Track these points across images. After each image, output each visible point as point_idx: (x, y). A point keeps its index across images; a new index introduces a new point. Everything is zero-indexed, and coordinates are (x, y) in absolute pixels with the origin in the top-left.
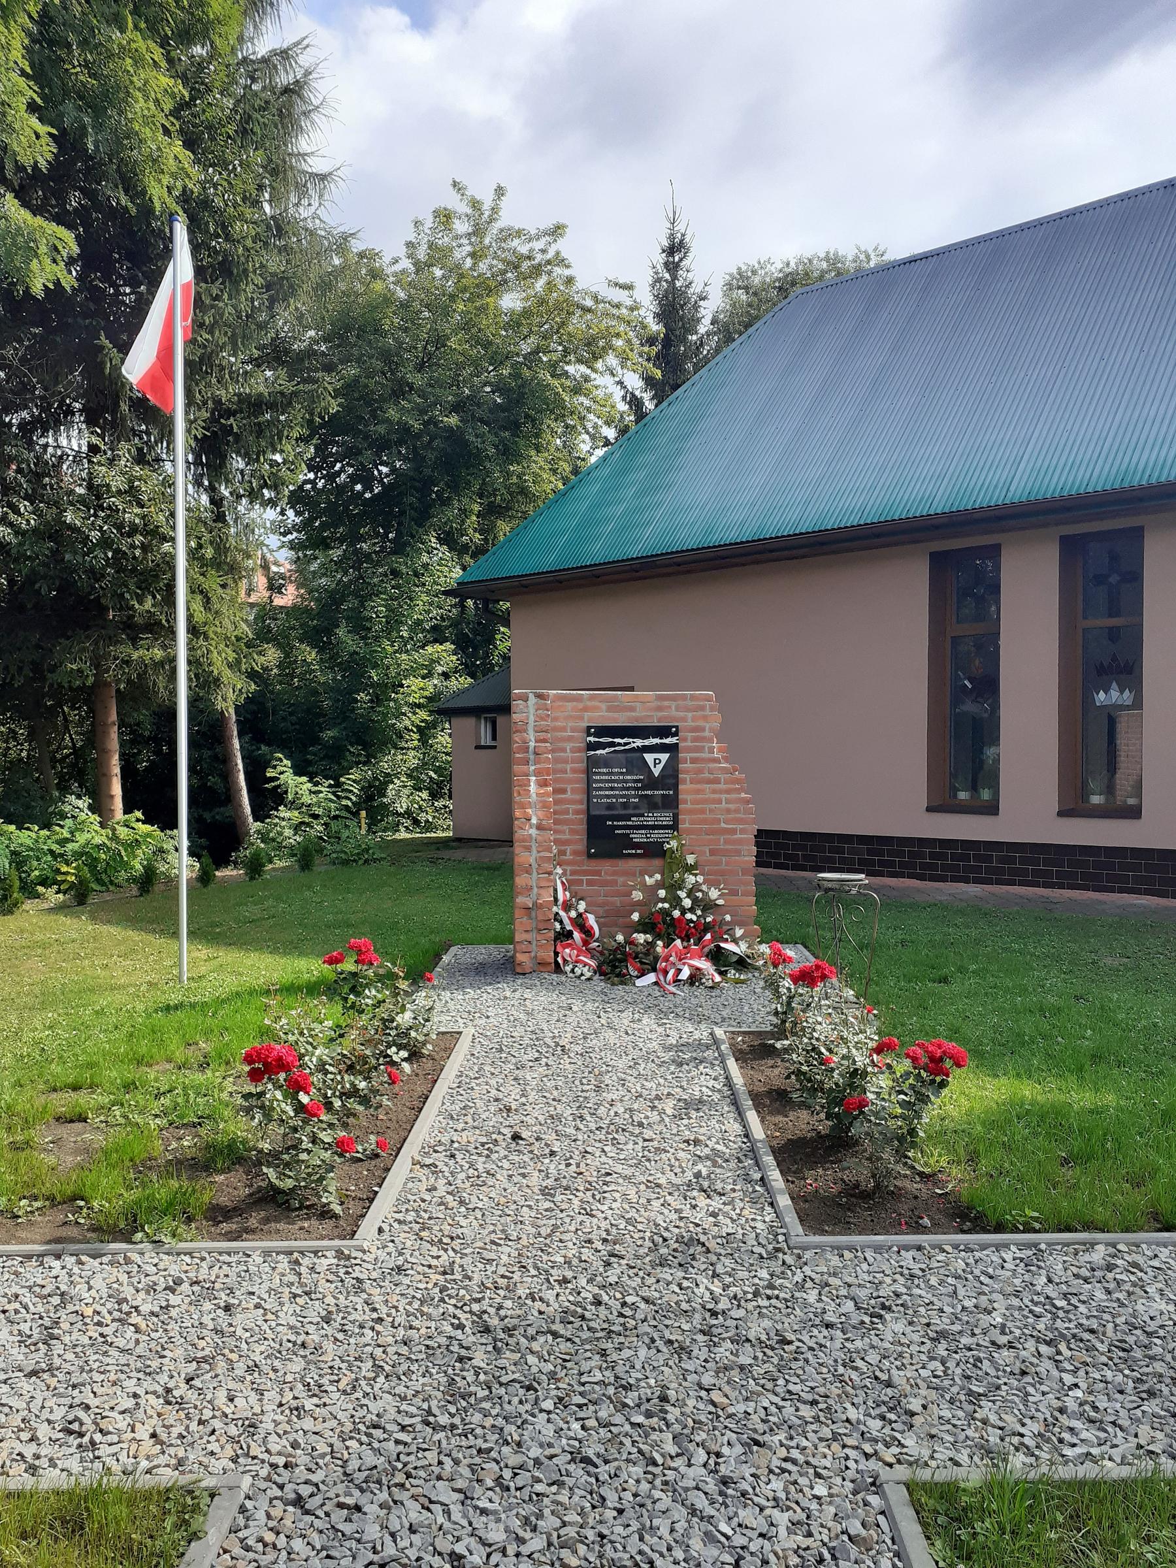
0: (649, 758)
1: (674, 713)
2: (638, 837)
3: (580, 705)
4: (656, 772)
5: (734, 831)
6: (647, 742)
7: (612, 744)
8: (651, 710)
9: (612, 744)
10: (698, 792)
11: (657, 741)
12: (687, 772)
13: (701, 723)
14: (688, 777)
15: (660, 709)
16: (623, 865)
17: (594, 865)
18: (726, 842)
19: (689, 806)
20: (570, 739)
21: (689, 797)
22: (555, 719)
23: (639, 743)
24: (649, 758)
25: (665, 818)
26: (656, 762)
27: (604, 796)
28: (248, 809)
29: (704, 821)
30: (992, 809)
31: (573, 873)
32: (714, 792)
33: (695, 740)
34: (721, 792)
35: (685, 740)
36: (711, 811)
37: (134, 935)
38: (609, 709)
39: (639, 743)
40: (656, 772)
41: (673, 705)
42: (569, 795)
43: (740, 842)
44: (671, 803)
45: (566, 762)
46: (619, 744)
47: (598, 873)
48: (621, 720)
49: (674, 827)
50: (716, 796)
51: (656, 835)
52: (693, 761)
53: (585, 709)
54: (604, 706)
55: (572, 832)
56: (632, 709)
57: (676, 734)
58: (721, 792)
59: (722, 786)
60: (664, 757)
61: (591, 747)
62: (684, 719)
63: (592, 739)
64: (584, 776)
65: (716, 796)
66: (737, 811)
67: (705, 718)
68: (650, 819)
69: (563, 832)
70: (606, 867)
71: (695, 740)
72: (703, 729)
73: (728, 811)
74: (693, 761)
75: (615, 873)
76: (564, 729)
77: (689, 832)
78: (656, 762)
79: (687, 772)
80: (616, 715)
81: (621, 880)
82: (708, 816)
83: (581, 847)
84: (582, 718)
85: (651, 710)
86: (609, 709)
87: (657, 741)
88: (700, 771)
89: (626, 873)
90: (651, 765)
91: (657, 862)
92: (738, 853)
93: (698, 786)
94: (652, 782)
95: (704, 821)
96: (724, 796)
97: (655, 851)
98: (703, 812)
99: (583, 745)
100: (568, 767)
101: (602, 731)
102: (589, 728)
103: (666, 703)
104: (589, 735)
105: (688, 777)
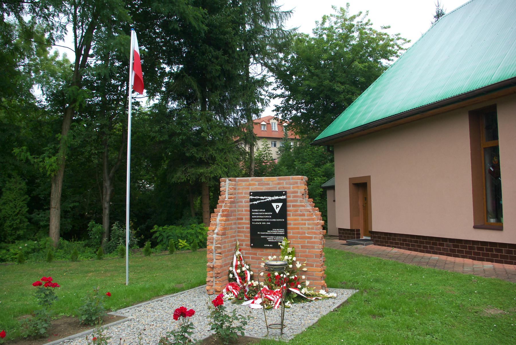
0: (274, 205)
1: (285, 186)
2: (270, 239)
3: (248, 183)
4: (277, 211)
5: (311, 238)
6: (273, 198)
7: (259, 199)
8: (275, 184)
9: (259, 199)
10: (295, 220)
11: (277, 198)
12: (290, 211)
13: (296, 190)
14: (291, 213)
15: (279, 184)
18: (308, 242)
20: (244, 197)
21: (292, 222)
22: (239, 189)
23: (270, 198)
24: (274, 205)
25: (281, 231)
26: (277, 207)
27: (258, 221)
29: (299, 233)
30: (500, 228)
31: (246, 254)
32: (302, 220)
33: (294, 197)
34: (305, 220)
35: (290, 197)
36: (302, 228)
38: (259, 184)
39: (270, 198)
40: (277, 211)
42: (244, 221)
43: (314, 242)
44: (284, 225)
45: (243, 207)
46: (262, 199)
47: (256, 254)
48: (264, 189)
49: (285, 235)
50: (304, 222)
52: (294, 206)
53: (250, 185)
54: (257, 183)
55: (245, 236)
56: (268, 184)
57: (285, 194)
58: (305, 220)
59: (306, 217)
60: (280, 205)
61: (252, 200)
62: (289, 188)
63: (252, 197)
65: (304, 222)
66: (312, 229)
67: (298, 187)
68: (275, 231)
69: (242, 236)
71: (294, 197)
72: (297, 192)
73: (309, 228)
74: (294, 206)
75: (262, 255)
76: (242, 193)
77: (293, 237)
79: (290, 211)
82: (300, 230)
83: (249, 243)
84: (248, 189)
85: (275, 184)
86: (259, 184)
87: (277, 198)
88: (297, 211)
90: (275, 208)
92: (313, 247)
93: (296, 217)
94: (275, 215)
95: (299, 233)
96: (307, 222)
98: (298, 228)
100: (244, 209)
101: (255, 194)
102: (250, 192)
103: (282, 181)
104: (250, 195)
105: (291, 213)
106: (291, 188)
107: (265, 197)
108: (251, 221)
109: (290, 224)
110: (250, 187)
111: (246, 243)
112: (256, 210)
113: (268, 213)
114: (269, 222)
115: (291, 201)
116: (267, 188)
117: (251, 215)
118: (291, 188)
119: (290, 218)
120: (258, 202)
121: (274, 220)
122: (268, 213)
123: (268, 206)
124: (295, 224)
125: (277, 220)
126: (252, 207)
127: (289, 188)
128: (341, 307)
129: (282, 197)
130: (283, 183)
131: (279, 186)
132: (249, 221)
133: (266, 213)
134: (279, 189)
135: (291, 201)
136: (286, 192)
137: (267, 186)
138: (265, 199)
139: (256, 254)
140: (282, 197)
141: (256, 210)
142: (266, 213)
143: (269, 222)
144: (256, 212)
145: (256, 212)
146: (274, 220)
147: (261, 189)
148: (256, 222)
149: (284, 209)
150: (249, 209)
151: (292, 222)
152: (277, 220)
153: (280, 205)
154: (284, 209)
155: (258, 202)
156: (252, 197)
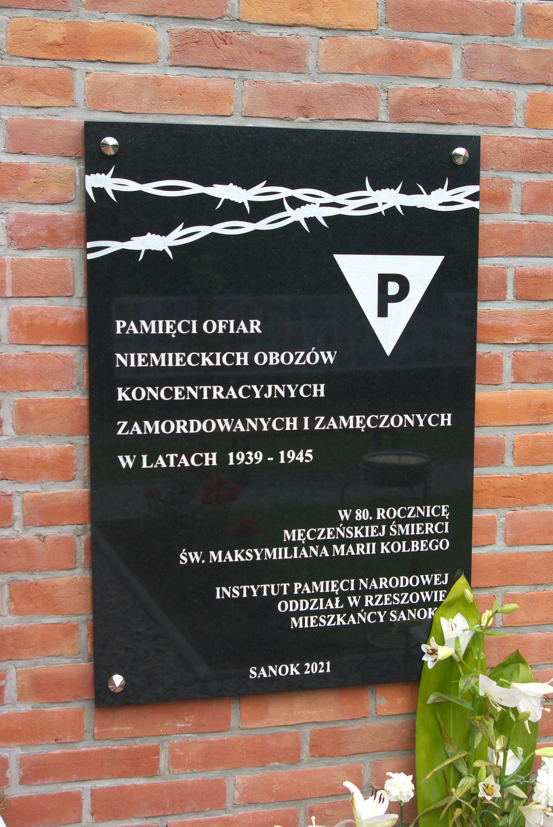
0: (360, 272)
1: (457, 83)
2: (308, 608)
4: (389, 331)
6: (350, 205)
8: (363, 64)
11: (390, 199)
12: (502, 334)
14: (506, 355)
15: (399, 62)
16: (241, 723)
17: (126, 733)
19: (508, 470)
21: (509, 436)
23: (316, 206)
24: (360, 272)
25: (421, 527)
27: (180, 441)
28: (140, 781)
35: (499, 200)
37: (300, 123)
38: (184, 52)
39: (316, 206)
40: (389, 331)
41: (457, 48)
44: (443, 471)
46: (233, 211)
47: (142, 762)
48: (241, 102)
49: (456, 560)
51: (384, 598)
56: (289, 58)
57: (467, 174)
60: (421, 270)
61: (104, 217)
62: (500, 114)
63: (108, 182)
64: (75, 355)
68: (359, 531)
70: (176, 740)
75: (212, 757)
77: (511, 572)
78: (392, 286)
79: (502, 334)
80: (216, 80)
81: (237, 781)
83: (73, 659)
84: (63, 89)
85: (363, 64)
86: (184, 52)
87: (390, 199)
89: (259, 754)
90: (367, 298)
91: (380, 709)
94: (365, 376)
97: (384, 657)
99: (71, 212)
101: (148, 148)
102: (93, 131)
103: (427, 40)
104: (96, 162)
105: (506, 355)
106: (519, 117)
107: (257, 193)
108: (103, 447)
109: (496, 456)
110: (84, 76)
111: (42, 664)
112: (168, 327)
113: (298, 358)
114: (297, 440)
115: (516, 242)
116: (273, 97)
117: (102, 377)
118: (519, 117)
119: (498, 392)
120: (177, 237)
121: (356, 422)
122: (298, 358)
123: (294, 278)
124: (533, 454)
125: (387, 421)
126: (112, 288)
127: (500, 114)
128: (197, 810)
129: (434, 200)
130: (442, 57)
131: (402, 86)
132: (78, 446)
133: (274, 358)
134: (399, 113)
135: (516, 242)
136: (472, 143)
137: (270, 78)
138: (260, 210)
139: (142, 762)
140: (434, 200)
141: (168, 327)
142: (274, 358)
143: (297, 440)
144: (161, 343)
145: (161, 343)
146: (356, 422)
147: (213, 99)
148: (156, 445)
149: (451, 307)
150: (72, 306)
151: (509, 436)
152: (387, 421)
153: (421, 270)
154: (451, 307)
155: (177, 237)
156: (108, 182)
